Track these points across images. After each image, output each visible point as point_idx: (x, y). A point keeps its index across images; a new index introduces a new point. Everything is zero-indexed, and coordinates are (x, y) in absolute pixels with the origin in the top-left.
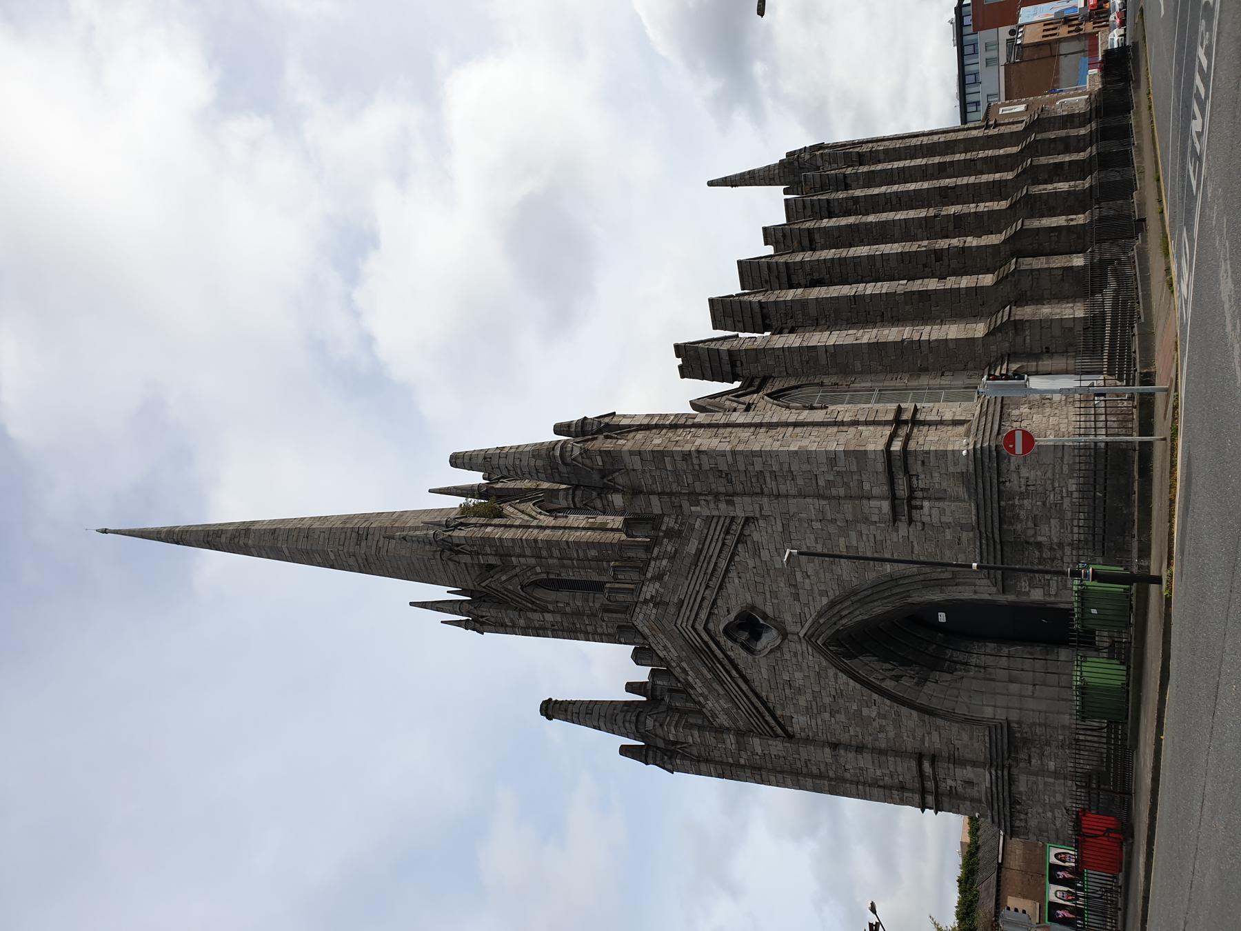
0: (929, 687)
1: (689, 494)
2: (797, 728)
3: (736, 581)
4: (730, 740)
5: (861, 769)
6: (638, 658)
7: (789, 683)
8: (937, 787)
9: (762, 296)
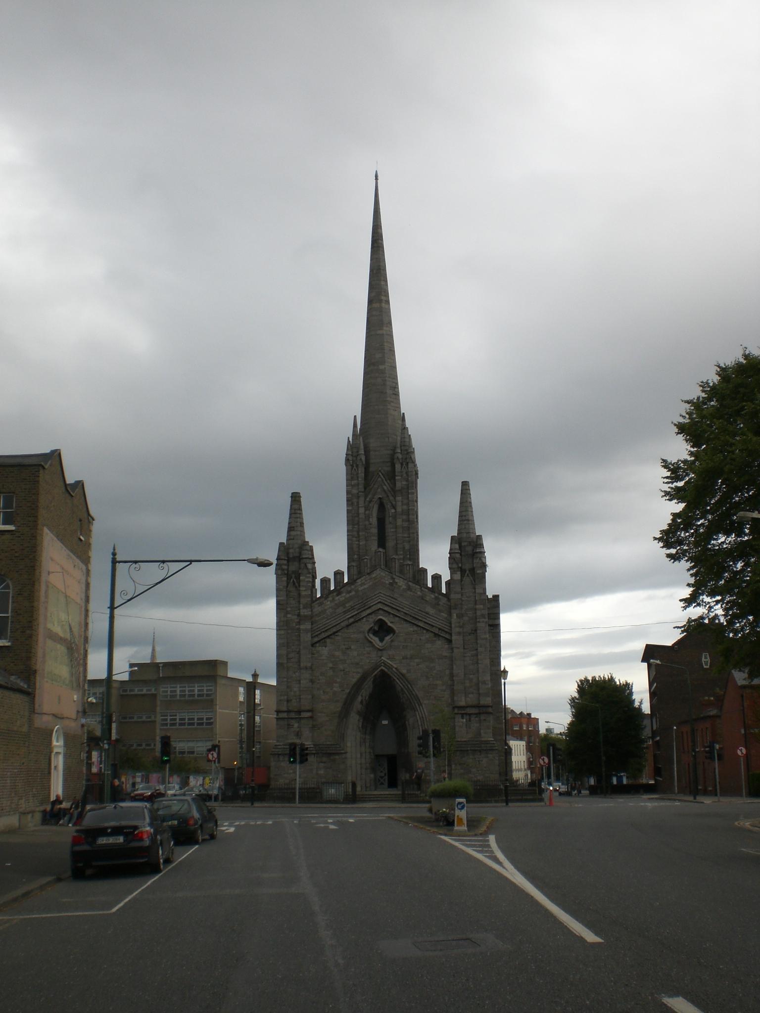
0: (357, 717)
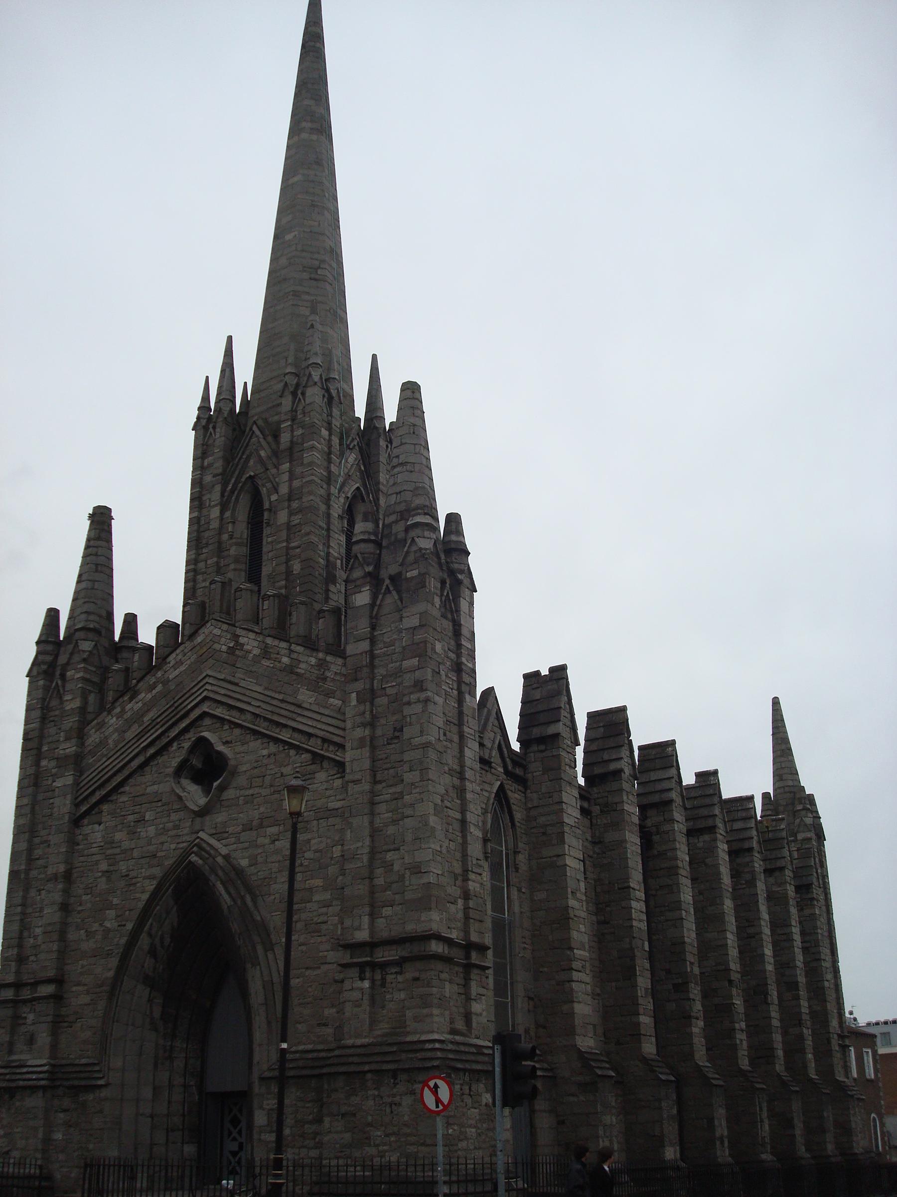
1: (372, 690)
2: (87, 830)
3: (265, 752)
4: (68, 748)
5: (41, 910)
6: (166, 629)
7: (141, 820)
8: (25, 1002)
9: (630, 774)
